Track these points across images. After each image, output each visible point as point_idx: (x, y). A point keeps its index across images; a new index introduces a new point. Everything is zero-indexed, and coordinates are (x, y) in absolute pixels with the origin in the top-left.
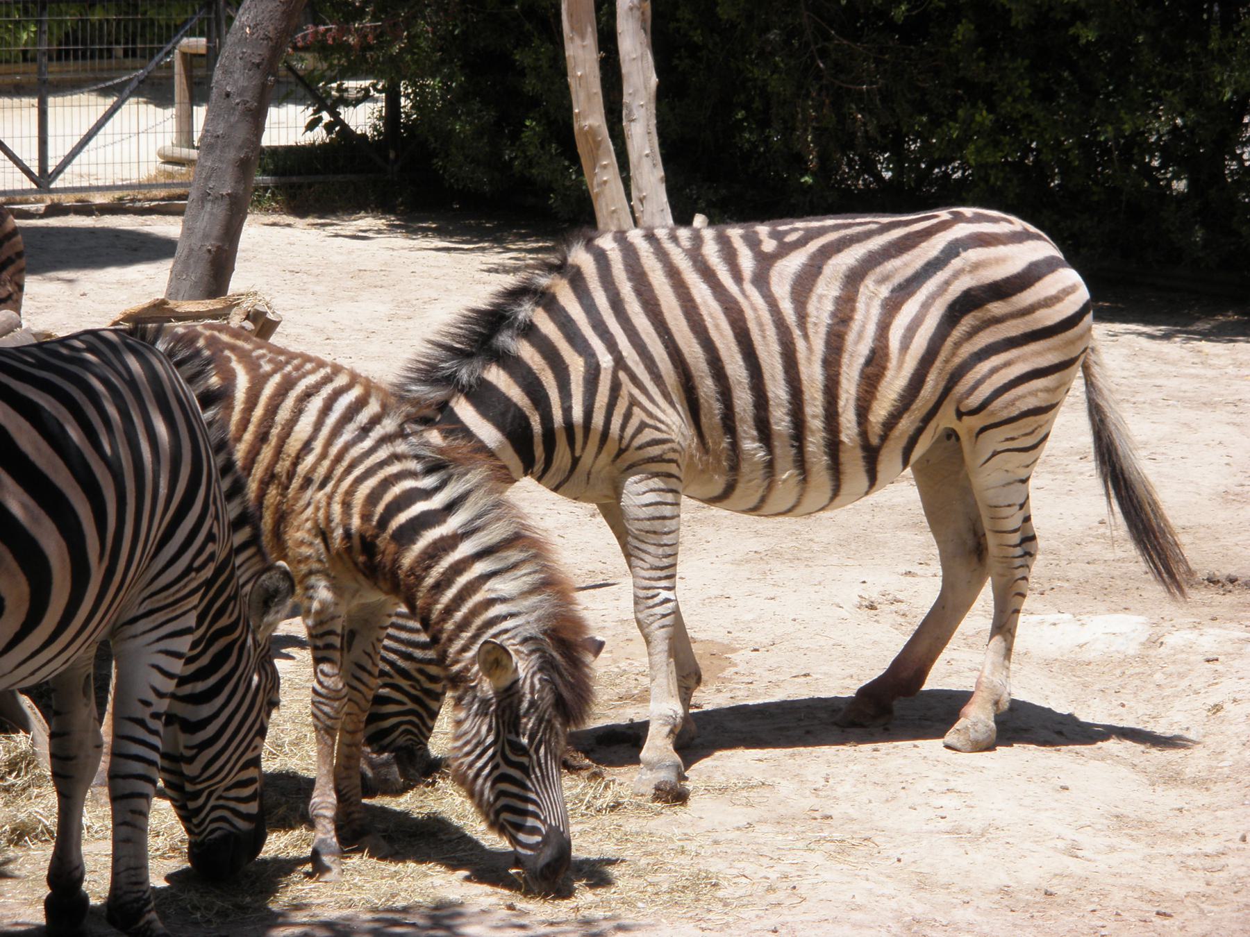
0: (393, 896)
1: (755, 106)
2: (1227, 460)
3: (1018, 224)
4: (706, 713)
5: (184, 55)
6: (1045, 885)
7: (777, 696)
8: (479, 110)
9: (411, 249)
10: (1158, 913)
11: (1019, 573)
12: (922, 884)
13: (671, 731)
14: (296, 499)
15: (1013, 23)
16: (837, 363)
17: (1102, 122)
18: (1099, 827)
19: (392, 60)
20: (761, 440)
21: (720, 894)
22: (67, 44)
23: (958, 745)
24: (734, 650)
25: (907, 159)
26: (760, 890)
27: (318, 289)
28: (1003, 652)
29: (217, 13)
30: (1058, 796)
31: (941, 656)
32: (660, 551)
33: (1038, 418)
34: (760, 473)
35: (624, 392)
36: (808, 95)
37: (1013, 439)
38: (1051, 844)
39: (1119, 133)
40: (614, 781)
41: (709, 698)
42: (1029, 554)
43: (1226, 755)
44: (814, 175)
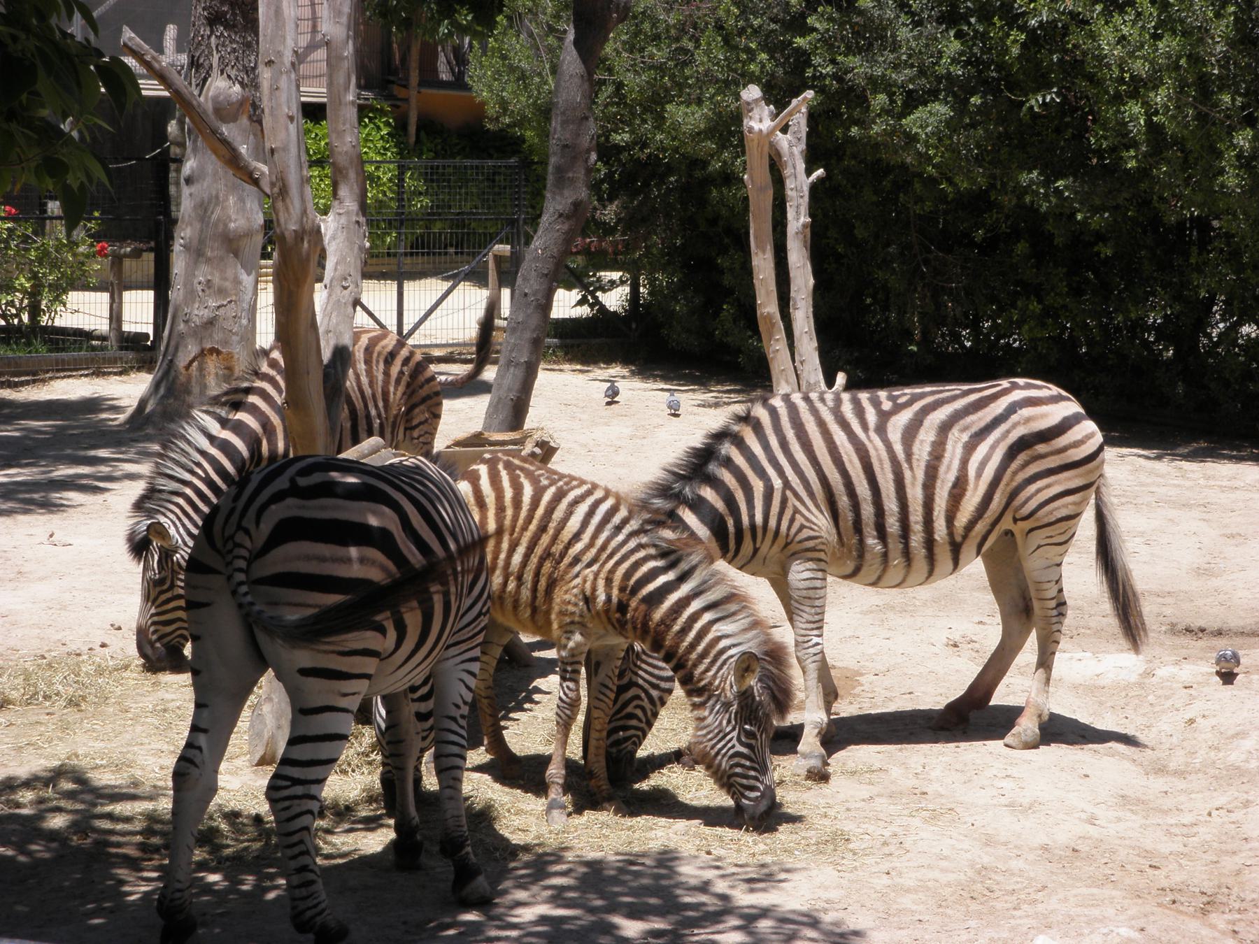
0: (630, 843)
1: (879, 296)
2: (1199, 545)
3: (1055, 390)
4: (843, 719)
5: (495, 256)
6: (1073, 845)
7: (891, 708)
8: (693, 297)
9: (645, 390)
10: (1150, 866)
11: (1055, 627)
12: (989, 842)
13: (819, 733)
14: (566, 572)
15: (1055, 243)
16: (933, 487)
17: (1116, 310)
18: (1110, 804)
19: (635, 262)
20: (879, 538)
21: (851, 846)
22: (417, 248)
23: (1014, 745)
24: (862, 675)
25: (982, 333)
26: (878, 844)
27: (585, 417)
28: (1044, 681)
29: (518, 230)
30: (1081, 781)
31: (1003, 682)
32: (813, 611)
33: (1068, 522)
34: (879, 560)
35: (790, 504)
36: (915, 290)
37: (1051, 537)
38: (1077, 815)
39: (1127, 319)
40: (779, 765)
41: (845, 708)
42: (1062, 615)
43: (1198, 755)
44: (917, 344)
